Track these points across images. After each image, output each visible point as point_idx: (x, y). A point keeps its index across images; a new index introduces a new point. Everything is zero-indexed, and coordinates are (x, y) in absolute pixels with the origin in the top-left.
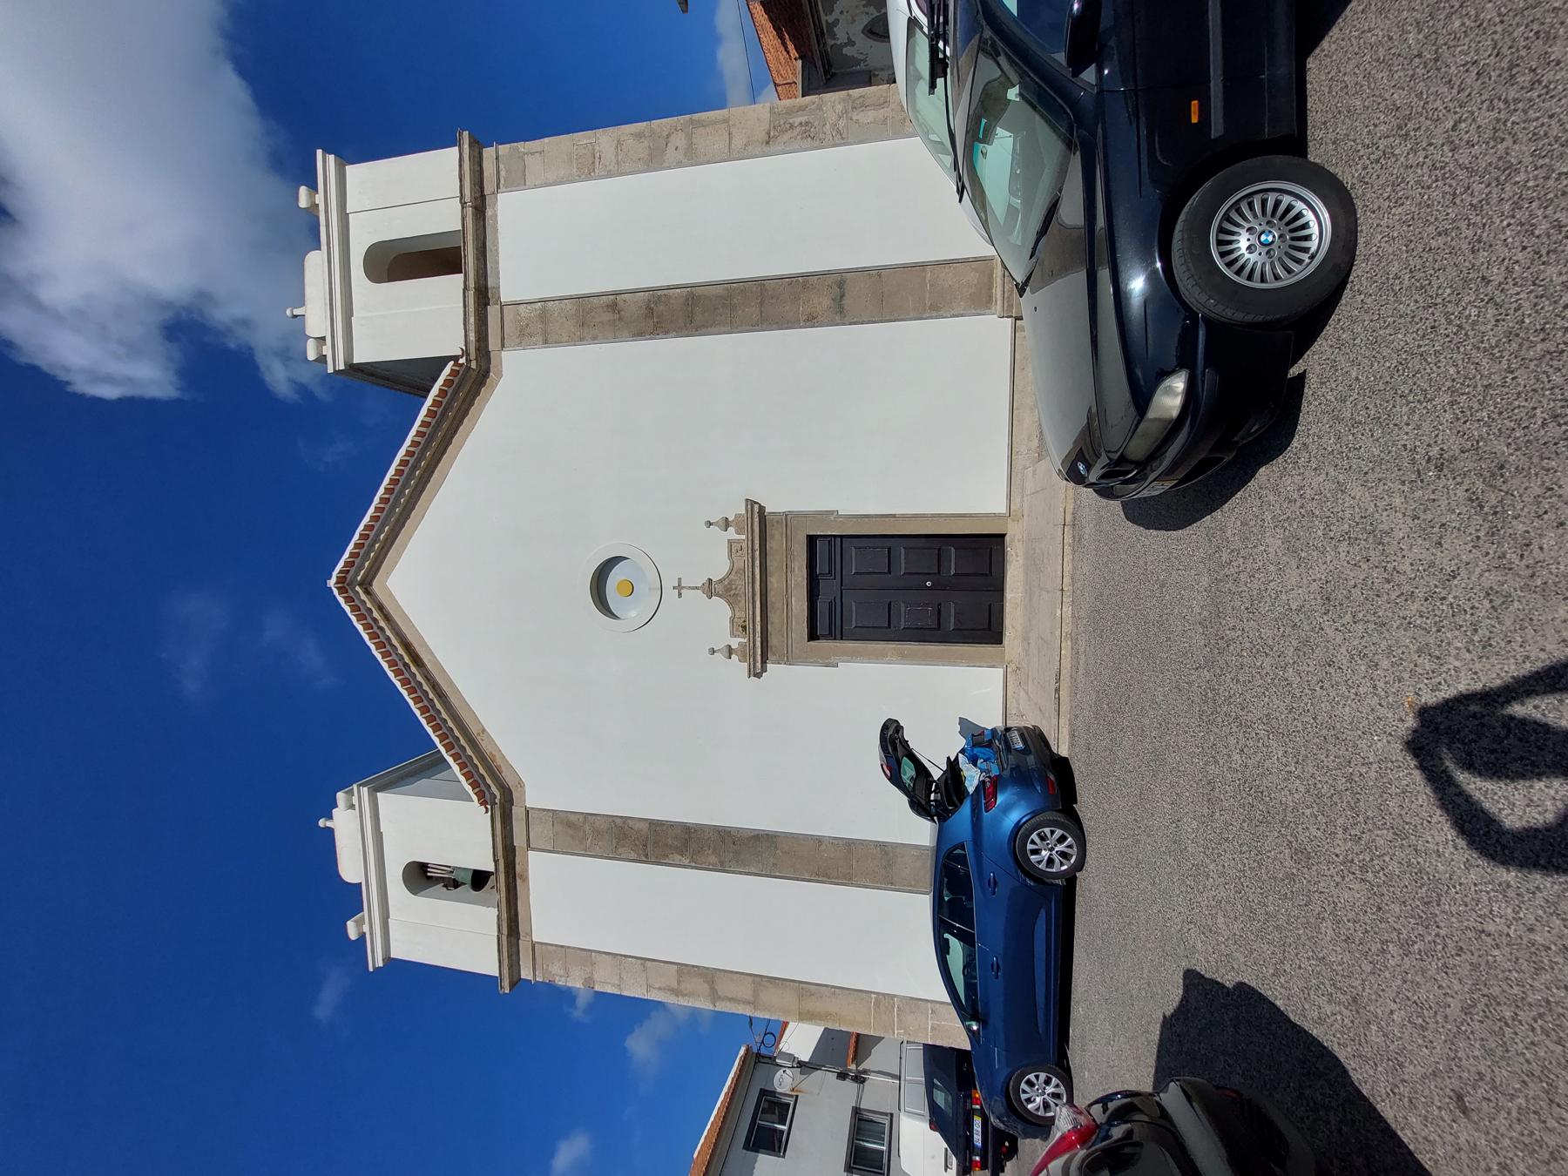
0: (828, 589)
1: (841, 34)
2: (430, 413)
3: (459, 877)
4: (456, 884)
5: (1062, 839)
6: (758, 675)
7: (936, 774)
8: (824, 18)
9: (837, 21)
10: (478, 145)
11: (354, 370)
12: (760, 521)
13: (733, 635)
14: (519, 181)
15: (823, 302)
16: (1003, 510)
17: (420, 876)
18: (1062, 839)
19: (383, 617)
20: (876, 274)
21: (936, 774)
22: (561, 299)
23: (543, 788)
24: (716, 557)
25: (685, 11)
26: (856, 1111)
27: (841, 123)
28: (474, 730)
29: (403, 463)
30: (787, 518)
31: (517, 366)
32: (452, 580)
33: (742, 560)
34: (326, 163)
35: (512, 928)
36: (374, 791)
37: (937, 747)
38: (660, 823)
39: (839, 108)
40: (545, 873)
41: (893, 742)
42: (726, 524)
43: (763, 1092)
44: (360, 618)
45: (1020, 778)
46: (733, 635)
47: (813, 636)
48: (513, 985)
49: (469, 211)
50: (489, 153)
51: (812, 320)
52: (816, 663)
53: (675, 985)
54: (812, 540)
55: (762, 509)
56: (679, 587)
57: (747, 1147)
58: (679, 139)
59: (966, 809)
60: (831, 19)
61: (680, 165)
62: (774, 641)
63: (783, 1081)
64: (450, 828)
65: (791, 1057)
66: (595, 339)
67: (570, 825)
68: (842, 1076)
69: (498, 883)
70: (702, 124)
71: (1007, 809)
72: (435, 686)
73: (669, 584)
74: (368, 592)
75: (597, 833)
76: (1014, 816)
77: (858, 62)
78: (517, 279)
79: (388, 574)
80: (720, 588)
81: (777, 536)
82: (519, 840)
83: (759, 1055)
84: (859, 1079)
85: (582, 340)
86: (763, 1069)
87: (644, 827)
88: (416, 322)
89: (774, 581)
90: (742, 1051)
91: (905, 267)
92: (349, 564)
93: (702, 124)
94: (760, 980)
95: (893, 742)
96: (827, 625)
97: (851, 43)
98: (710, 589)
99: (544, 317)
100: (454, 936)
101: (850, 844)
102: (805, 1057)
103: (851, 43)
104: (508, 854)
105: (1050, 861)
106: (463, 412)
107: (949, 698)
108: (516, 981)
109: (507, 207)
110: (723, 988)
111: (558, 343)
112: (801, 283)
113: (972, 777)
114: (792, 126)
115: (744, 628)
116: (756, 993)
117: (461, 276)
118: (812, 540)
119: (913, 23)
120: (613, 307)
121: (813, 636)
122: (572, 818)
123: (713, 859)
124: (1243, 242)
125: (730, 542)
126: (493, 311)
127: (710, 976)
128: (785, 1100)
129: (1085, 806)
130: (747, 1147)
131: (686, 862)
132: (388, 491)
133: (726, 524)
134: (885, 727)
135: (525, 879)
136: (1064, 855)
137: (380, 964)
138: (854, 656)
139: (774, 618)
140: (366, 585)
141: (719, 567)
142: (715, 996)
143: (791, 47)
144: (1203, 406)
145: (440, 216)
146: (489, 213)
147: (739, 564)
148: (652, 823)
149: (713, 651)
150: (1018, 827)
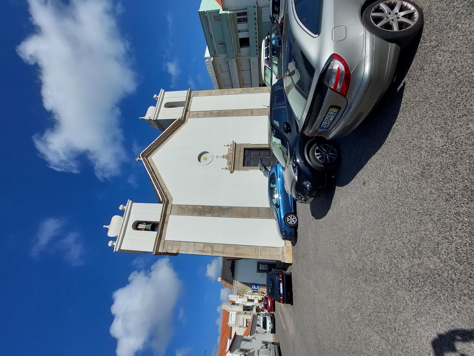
0: (247, 158)
12: (235, 146)
15: (249, 113)
19: (148, 163)
23: (177, 198)
24: (226, 151)
30: (241, 145)
31: (190, 122)
33: (231, 152)
34: (162, 91)
42: (228, 146)
47: (244, 166)
50: (192, 92)
53: (202, 249)
62: (236, 167)
64: (150, 211)
67: (182, 208)
73: (215, 156)
75: (189, 210)
85: (204, 117)
88: (176, 114)
89: (236, 156)
98: (223, 157)
101: (250, 208)
110: (215, 249)
120: (211, 113)
121: (244, 166)
122: (183, 206)
123: (217, 214)
126: (188, 113)
133: (228, 146)
135: (167, 223)
137: (117, 250)
138: (252, 169)
141: (226, 153)
142: (213, 251)
147: (230, 152)
148: (203, 206)
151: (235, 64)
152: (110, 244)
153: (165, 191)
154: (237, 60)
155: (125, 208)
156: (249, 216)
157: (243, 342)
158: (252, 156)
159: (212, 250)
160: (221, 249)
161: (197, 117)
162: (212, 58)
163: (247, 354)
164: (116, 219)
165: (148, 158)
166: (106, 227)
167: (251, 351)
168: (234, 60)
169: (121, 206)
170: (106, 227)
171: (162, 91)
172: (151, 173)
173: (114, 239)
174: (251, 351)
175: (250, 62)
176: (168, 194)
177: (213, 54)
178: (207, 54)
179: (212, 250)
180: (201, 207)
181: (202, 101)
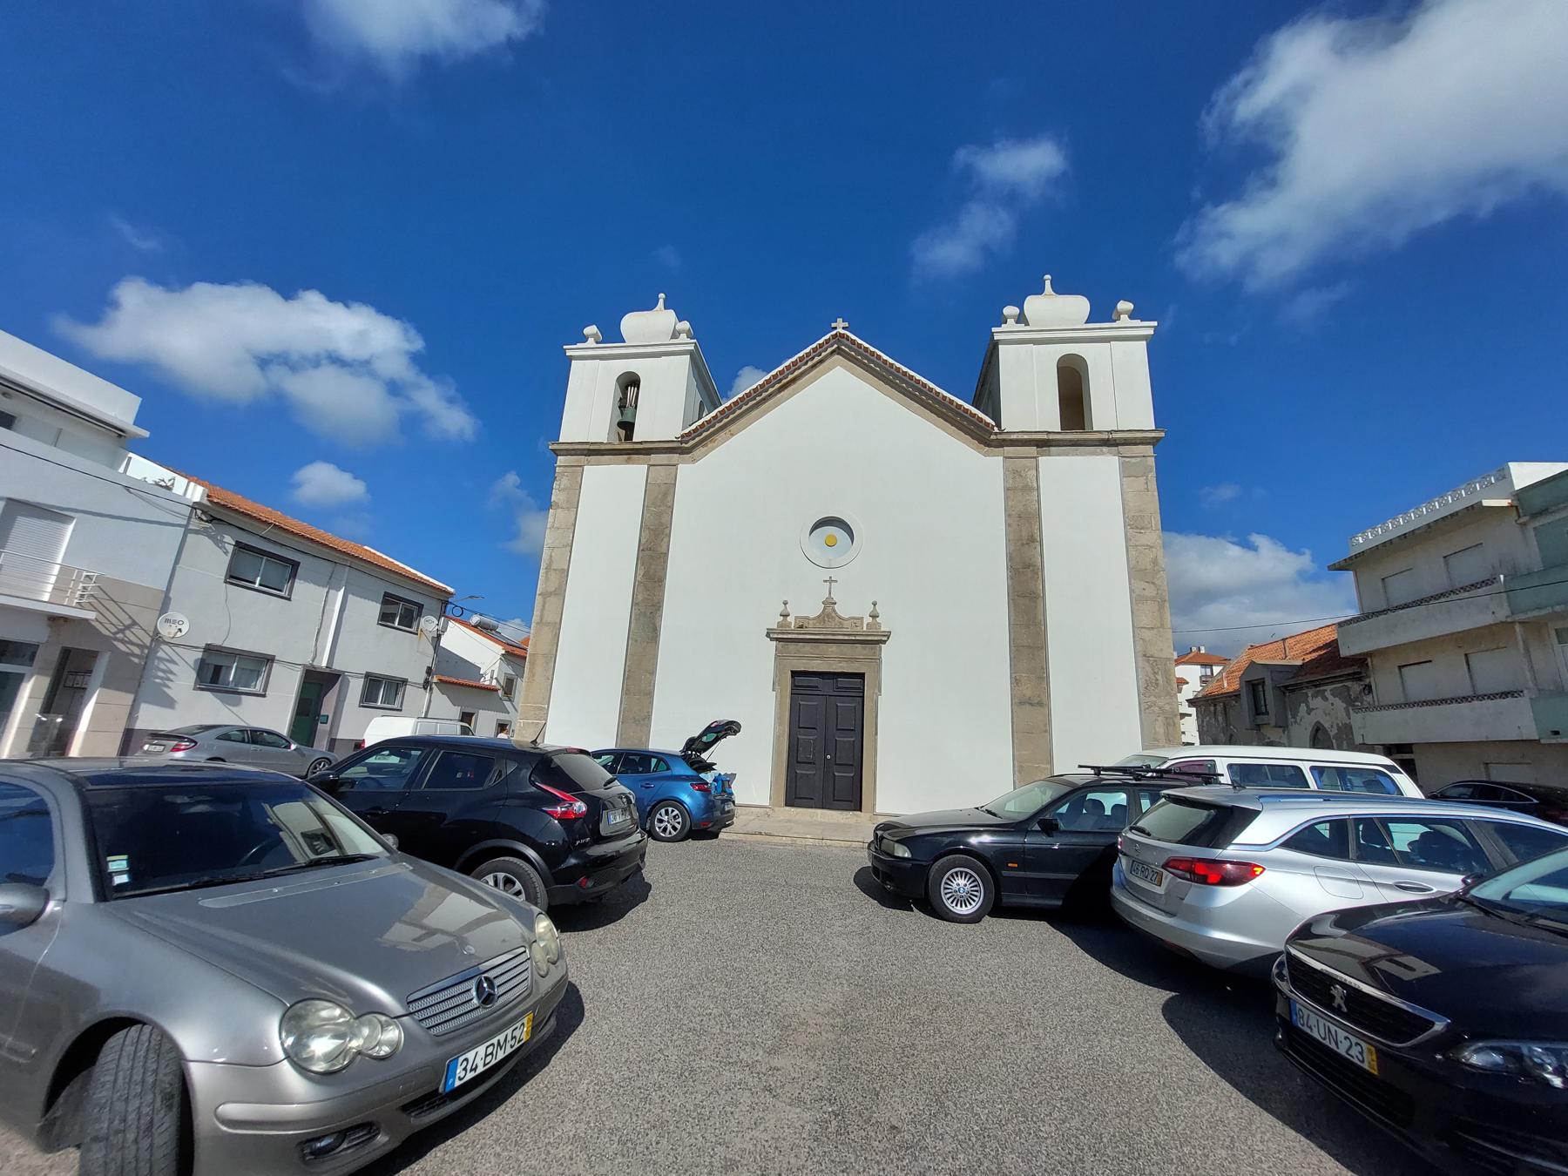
0: (826, 686)
1: (1317, 702)
2: (959, 406)
3: (628, 411)
4: (622, 407)
5: (674, 828)
6: (768, 635)
7: (704, 756)
8: (1329, 688)
9: (1326, 699)
10: (1154, 442)
11: (995, 346)
12: (875, 641)
14: (1126, 472)
15: (1028, 691)
16: (878, 811)
17: (630, 382)
18: (674, 828)
19: (816, 363)
20: (1046, 728)
21: (704, 756)
22: (1039, 501)
23: (688, 473)
24: (851, 607)
25: (1330, 568)
26: (404, 682)
28: (733, 428)
29: (924, 385)
30: (876, 661)
31: (990, 467)
32: (840, 418)
34: (1147, 328)
35: (593, 452)
36: (691, 353)
37: (721, 756)
38: (666, 562)
40: (633, 475)
41: (726, 729)
42: (874, 616)
43: (421, 607)
44: (815, 350)
45: (709, 807)
47: (794, 674)
48: (554, 450)
49: (1105, 436)
50: (1149, 450)
51: (1015, 681)
52: (776, 675)
54: (861, 676)
56: (831, 581)
57: (386, 594)
58: (1150, 591)
59: (690, 772)
60: (1328, 694)
61: (1132, 591)
62: (792, 646)
63: (428, 623)
64: (664, 410)
65: (444, 629)
66: (1008, 525)
67: (665, 495)
68: (429, 671)
69: (625, 441)
70: (1161, 608)
71: (690, 795)
72: (764, 400)
73: (834, 574)
75: (659, 515)
76: (686, 799)
77: (1294, 717)
78: (1054, 469)
79: (845, 367)
80: (829, 610)
82: (655, 458)
83: (447, 603)
84: (426, 685)
85: (1008, 516)
86: (437, 606)
87: (663, 549)
88: (1027, 399)
89: (833, 648)
90: (450, 589)
91: (1051, 750)
92: (853, 342)
93: (1161, 608)
94: (556, 628)
95: (726, 729)
96: (803, 685)
97: (1309, 711)
98: (829, 603)
99: (1027, 489)
100: (586, 411)
101: (650, 694)
103: (1309, 711)
104: (646, 450)
105: (661, 821)
106: (960, 427)
107: (752, 769)
108: (556, 453)
109: (1107, 464)
110: (552, 600)
111: (1007, 498)
112: (1042, 676)
113: (708, 777)
117: (1056, 425)
118: (861, 676)
119: (1165, 760)
120: (1032, 539)
121: (794, 674)
123: (640, 598)
124: (962, 881)
126: (1033, 450)
127: (560, 592)
128: (415, 624)
129: (690, 842)
130: (386, 594)
132: (905, 373)
133: (874, 616)
134: (732, 722)
135: (627, 462)
136: (665, 830)
137: (569, 353)
138: (779, 703)
139: (808, 647)
141: (843, 610)
142: (545, 595)
143: (1315, 655)
144: (905, 873)
145: (1104, 415)
146: (1105, 449)
147: (846, 624)
148: (666, 554)
149: (785, 603)
150: (682, 803)
151: (1485, 619)
152: (1010, 310)
154: (1506, 626)
155: (1124, 317)
156: (626, 691)
159: (551, 594)
160: (549, 617)
161: (1007, 489)
162: (1505, 503)
163: (500, 693)
164: (1078, 306)
165: (836, 357)
166: (1048, 284)
168: (1503, 613)
169: (1130, 306)
170: (1048, 284)
171: (1147, 328)
173: (1021, 319)
174: (507, 704)
175: (1504, 695)
177: (1531, 504)
178: (1525, 474)
179: (551, 594)
180: (663, 549)
181: (1091, 502)
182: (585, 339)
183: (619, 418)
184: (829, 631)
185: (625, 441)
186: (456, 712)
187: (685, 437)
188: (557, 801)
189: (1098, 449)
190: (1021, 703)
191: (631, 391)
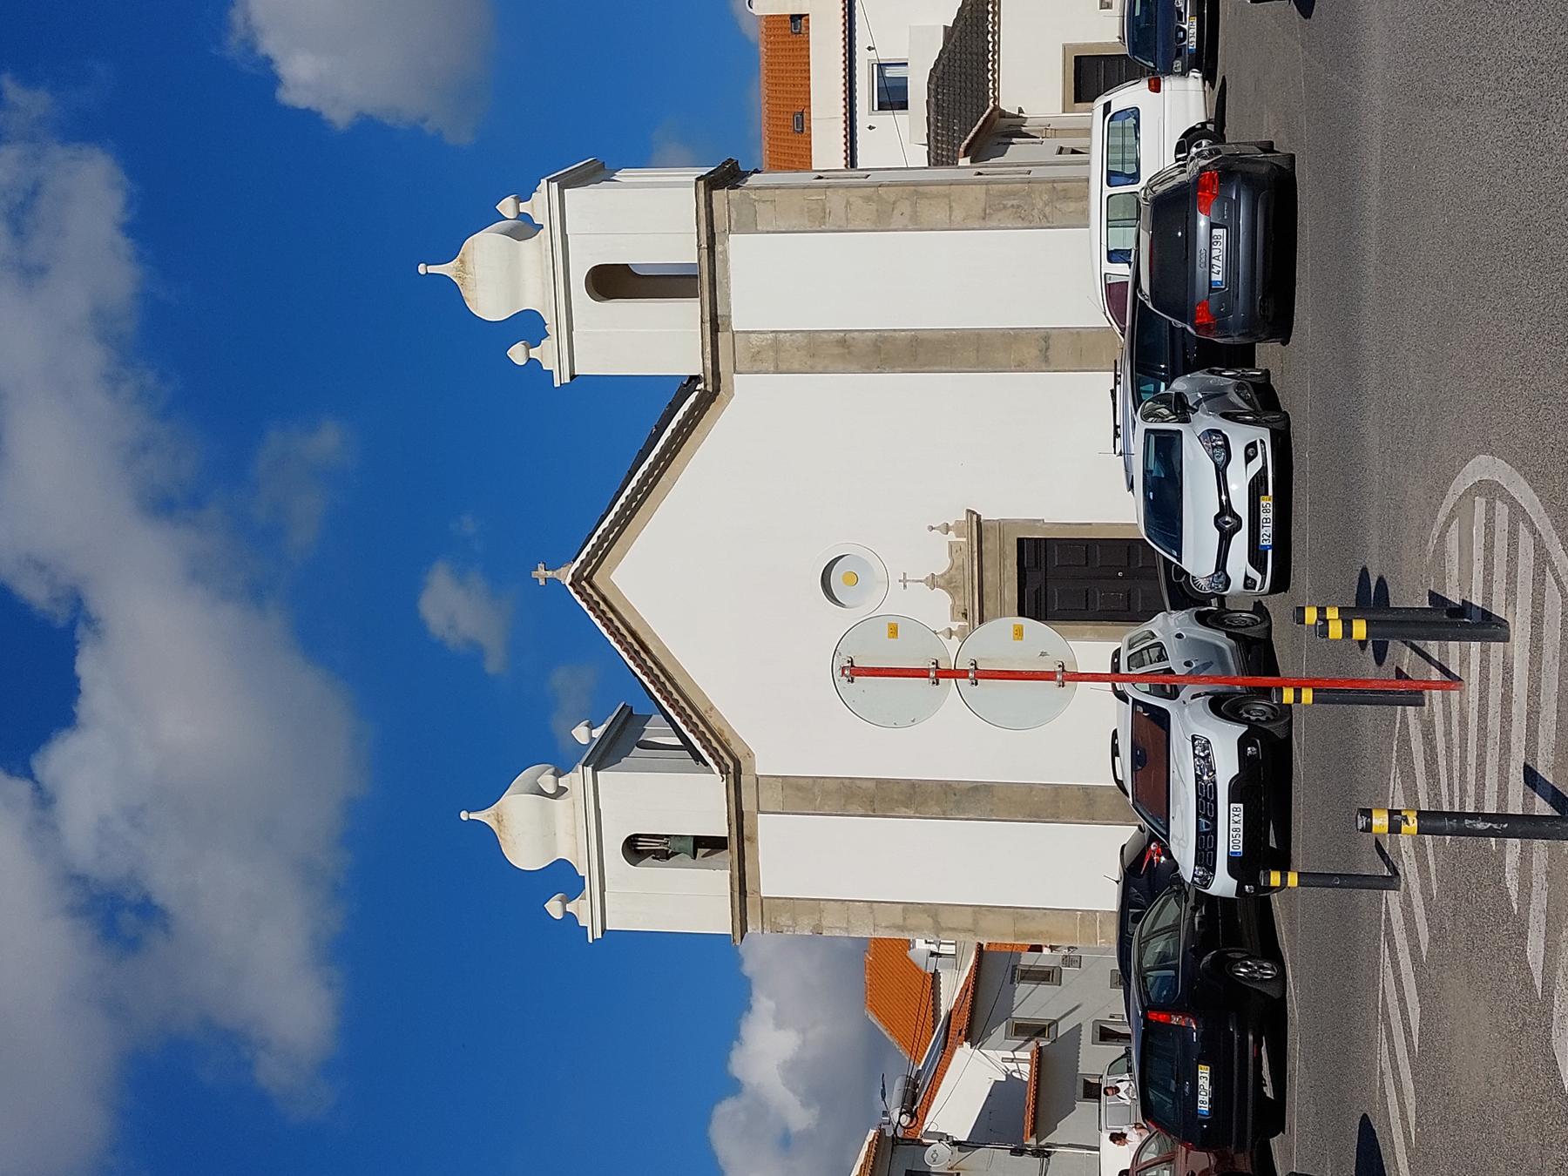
3: (672, 846)
4: (665, 856)
13: (953, 619)
14: (750, 227)
15: (1031, 352)
17: (635, 849)
19: (605, 607)
23: (769, 758)
24: (938, 556)
27: (1047, 210)
28: (702, 709)
30: (1001, 525)
31: (748, 393)
32: (691, 571)
33: (963, 558)
39: (1045, 197)
42: (947, 529)
46: (953, 619)
51: (1021, 367)
53: (900, 921)
54: (1020, 541)
55: (979, 517)
56: (904, 581)
58: (905, 207)
64: (690, 801)
65: (941, 1137)
67: (799, 788)
74: (592, 586)
78: (748, 311)
79: (611, 570)
80: (941, 582)
81: (991, 538)
87: (872, 785)
88: (656, 339)
89: (988, 576)
90: (872, 1132)
98: (933, 582)
100: (690, 901)
101: (1057, 788)
102: (963, 1136)
104: (738, 817)
109: (739, 249)
110: (945, 920)
114: (1005, 207)
115: (965, 615)
116: (976, 922)
118: (1020, 541)
122: (802, 782)
123: (936, 809)
125: (951, 545)
131: (911, 813)
133: (947, 529)
135: (753, 840)
140: (589, 580)
141: (942, 565)
145: (682, 250)
146: (719, 248)
148: (878, 781)
153: (711, 721)
156: (1056, 817)
157: (1022, 988)
158: (1060, 577)
159: (936, 922)
160: (967, 921)
167: (1063, 1028)
172: (635, 656)
174: (1063, 1028)
176: (727, 735)
179: (936, 922)
182: (570, 918)
183: (688, 858)
184: (968, 587)
185: (723, 847)
186: (1085, 1108)
187: (724, 771)
188: (1151, 859)
189: (718, 257)
190: (1046, 360)
191: (642, 845)
